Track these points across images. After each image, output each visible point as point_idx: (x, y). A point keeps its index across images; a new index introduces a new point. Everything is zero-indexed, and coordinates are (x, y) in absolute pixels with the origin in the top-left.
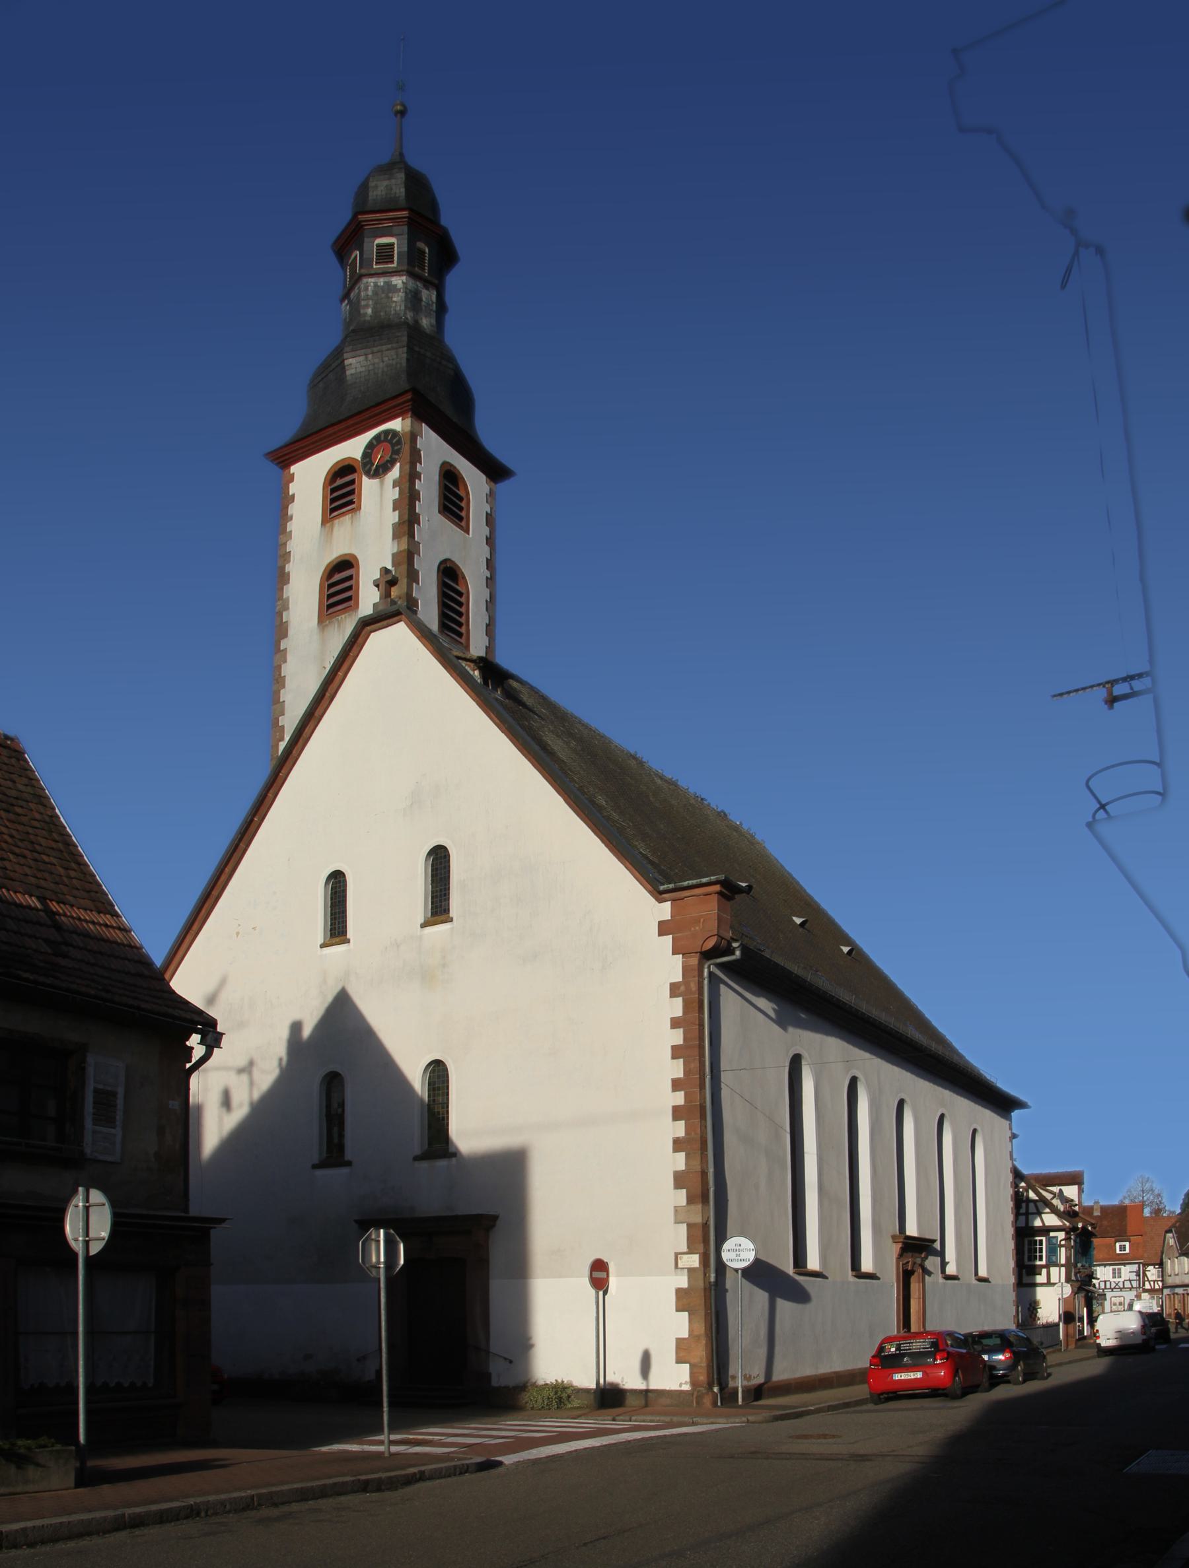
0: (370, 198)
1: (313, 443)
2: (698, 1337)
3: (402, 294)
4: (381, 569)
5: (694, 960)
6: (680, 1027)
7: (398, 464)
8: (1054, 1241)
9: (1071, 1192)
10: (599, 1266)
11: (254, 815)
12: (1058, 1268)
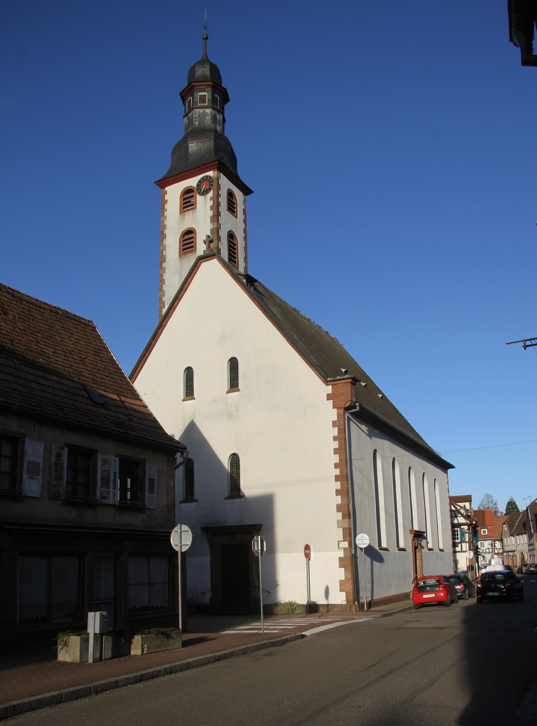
0: (196, 75)
1: (176, 179)
2: (349, 579)
3: (210, 117)
4: (206, 236)
5: (342, 411)
6: (337, 440)
7: (212, 191)
8: (463, 530)
9: (467, 505)
10: (307, 547)
11: (153, 341)
12: (465, 543)
